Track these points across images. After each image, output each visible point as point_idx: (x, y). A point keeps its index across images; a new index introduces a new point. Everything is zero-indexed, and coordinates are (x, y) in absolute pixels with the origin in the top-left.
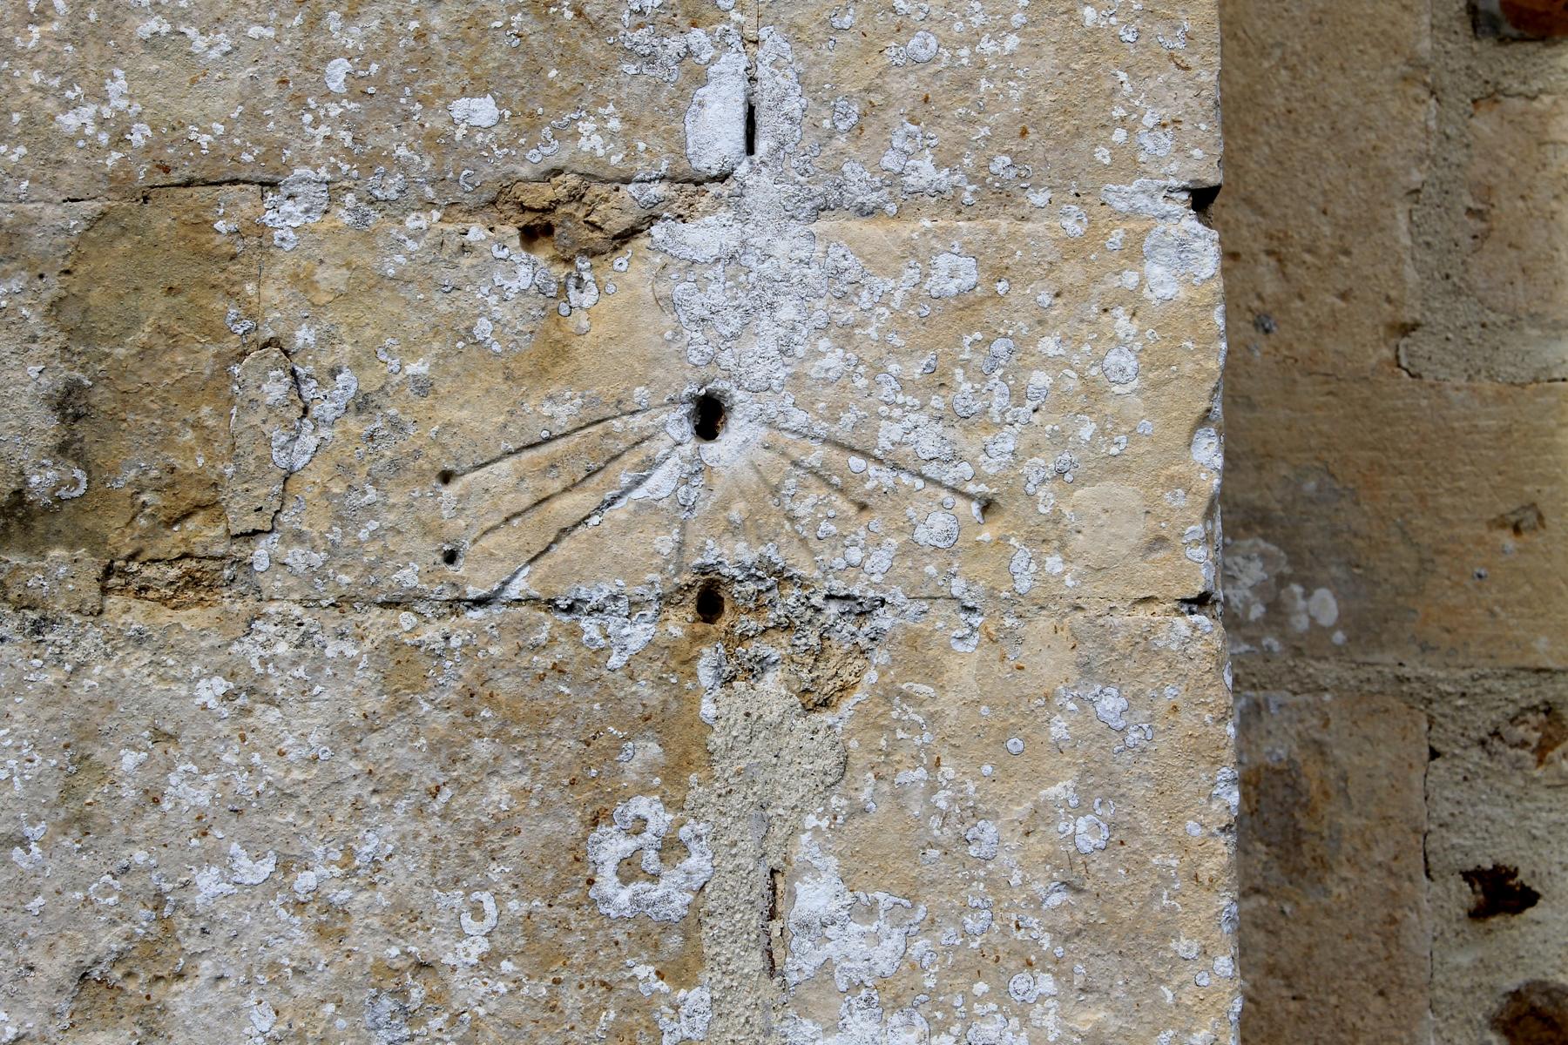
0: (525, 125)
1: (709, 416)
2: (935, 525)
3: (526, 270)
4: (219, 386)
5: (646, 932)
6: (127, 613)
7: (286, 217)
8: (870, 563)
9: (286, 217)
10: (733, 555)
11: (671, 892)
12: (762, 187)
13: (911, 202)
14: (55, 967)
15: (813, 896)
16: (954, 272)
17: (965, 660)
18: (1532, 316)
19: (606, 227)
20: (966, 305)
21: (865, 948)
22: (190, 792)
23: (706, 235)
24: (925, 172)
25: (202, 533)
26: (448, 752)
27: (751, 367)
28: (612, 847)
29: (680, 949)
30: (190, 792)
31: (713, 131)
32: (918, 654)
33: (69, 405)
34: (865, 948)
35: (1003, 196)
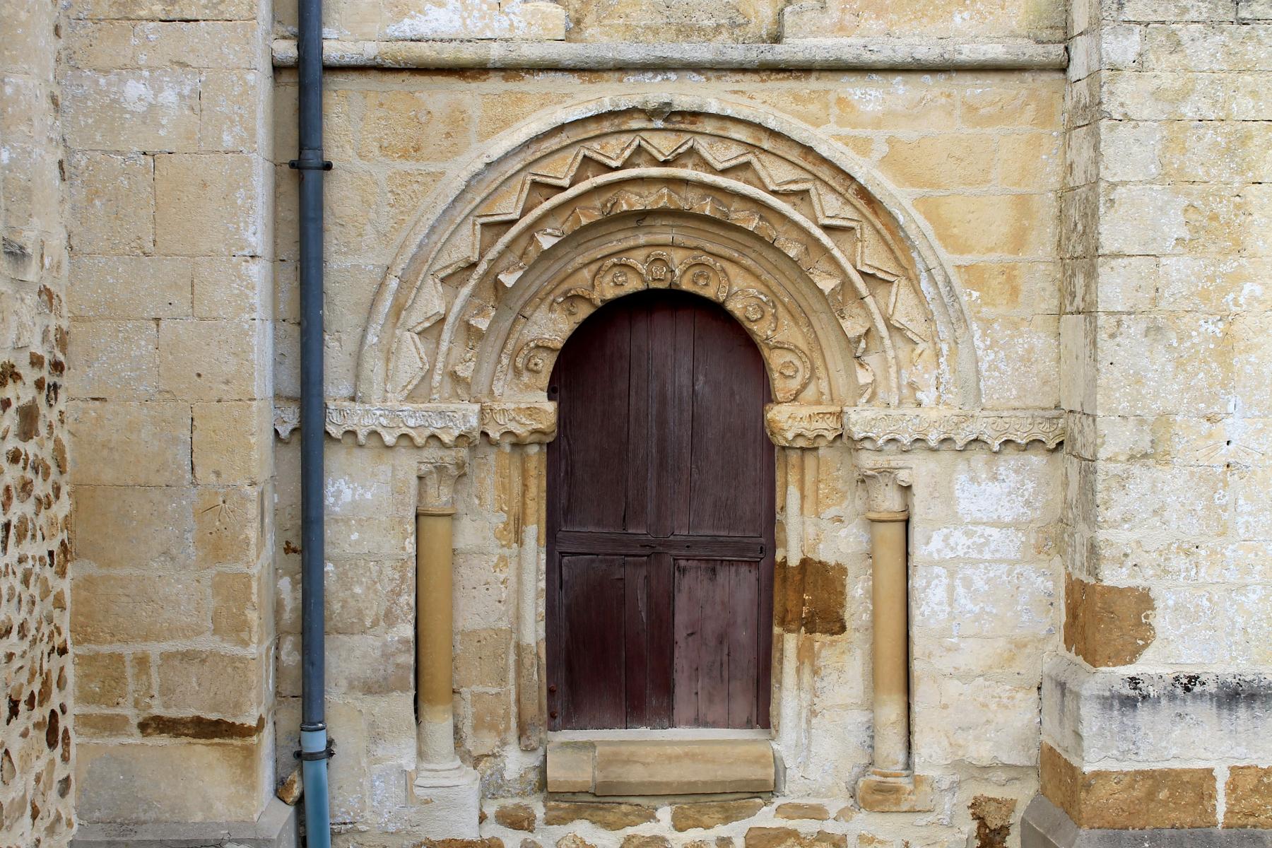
0: (1208, 407)
1: (1228, 443)
2: (1257, 457)
3: (1208, 425)
4: (1170, 440)
5: (1221, 506)
6: (1159, 467)
7: (1178, 418)
8: (1248, 461)
9: (1178, 418)
10: (1231, 460)
11: (1224, 501)
12: (1237, 415)
13: (1255, 417)
14: (1151, 509)
15: (1241, 502)
16: (1260, 426)
17: (1259, 471)
18: (1144, 698)
19: (1125, 352)
20: (1261, 430)
21: (1247, 508)
22: (1166, 489)
23: (1230, 421)
24: (1257, 413)
25: (1168, 457)
26: (1197, 484)
27: (1235, 438)
28: (1217, 496)
29: (1224, 508)
30: (1166, 489)
31: (1231, 408)
32: (1254, 472)
33: (1152, 442)
34: (1247, 508)
35: (1266, 416)
